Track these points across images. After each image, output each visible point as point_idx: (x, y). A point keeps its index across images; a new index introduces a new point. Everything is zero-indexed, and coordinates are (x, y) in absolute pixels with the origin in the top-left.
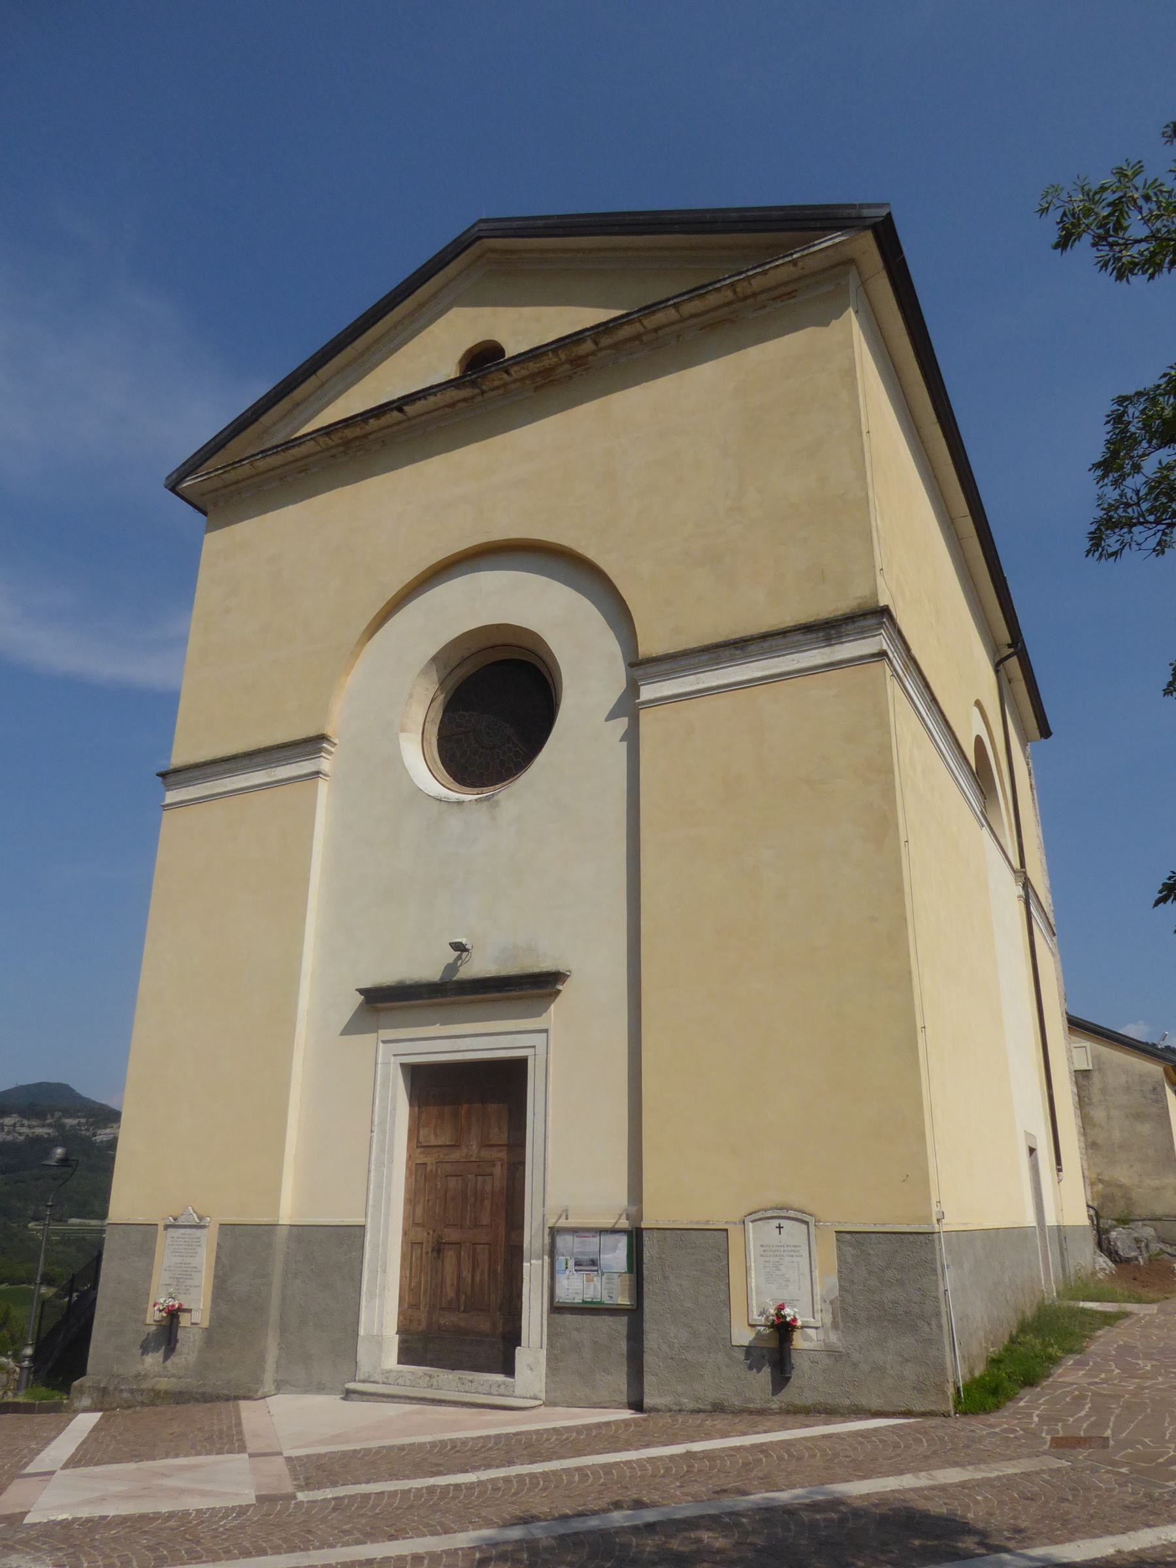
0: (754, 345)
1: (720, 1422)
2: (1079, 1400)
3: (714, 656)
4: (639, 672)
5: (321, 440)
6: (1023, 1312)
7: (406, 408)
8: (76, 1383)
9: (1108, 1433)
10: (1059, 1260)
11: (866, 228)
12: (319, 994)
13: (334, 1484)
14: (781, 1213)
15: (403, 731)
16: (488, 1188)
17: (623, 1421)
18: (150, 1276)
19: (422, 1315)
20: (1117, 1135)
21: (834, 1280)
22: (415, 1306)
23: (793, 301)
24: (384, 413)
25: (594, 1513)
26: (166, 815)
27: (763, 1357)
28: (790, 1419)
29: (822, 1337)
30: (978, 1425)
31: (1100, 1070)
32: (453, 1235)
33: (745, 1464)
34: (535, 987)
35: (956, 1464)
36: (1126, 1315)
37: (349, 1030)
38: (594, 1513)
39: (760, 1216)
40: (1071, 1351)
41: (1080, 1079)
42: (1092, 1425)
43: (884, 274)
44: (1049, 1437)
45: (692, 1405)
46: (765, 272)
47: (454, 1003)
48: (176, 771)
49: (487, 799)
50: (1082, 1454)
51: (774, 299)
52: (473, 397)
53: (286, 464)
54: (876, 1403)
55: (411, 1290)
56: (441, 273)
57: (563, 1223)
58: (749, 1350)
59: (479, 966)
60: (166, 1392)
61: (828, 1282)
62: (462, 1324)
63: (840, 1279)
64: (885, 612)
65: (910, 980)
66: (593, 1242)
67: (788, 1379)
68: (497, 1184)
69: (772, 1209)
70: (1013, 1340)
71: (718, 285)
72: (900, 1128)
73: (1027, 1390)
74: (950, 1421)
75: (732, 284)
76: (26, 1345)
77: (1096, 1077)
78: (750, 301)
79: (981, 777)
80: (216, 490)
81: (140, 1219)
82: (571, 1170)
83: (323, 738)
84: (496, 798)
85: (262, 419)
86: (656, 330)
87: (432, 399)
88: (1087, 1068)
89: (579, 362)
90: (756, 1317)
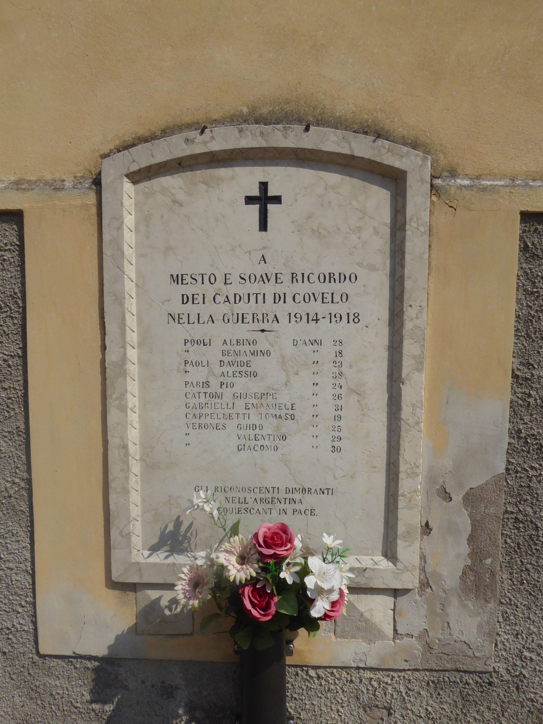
21: (491, 412)
27: (168, 692)
58: (107, 674)
61: (466, 424)
69: (236, 120)
90: (138, 553)
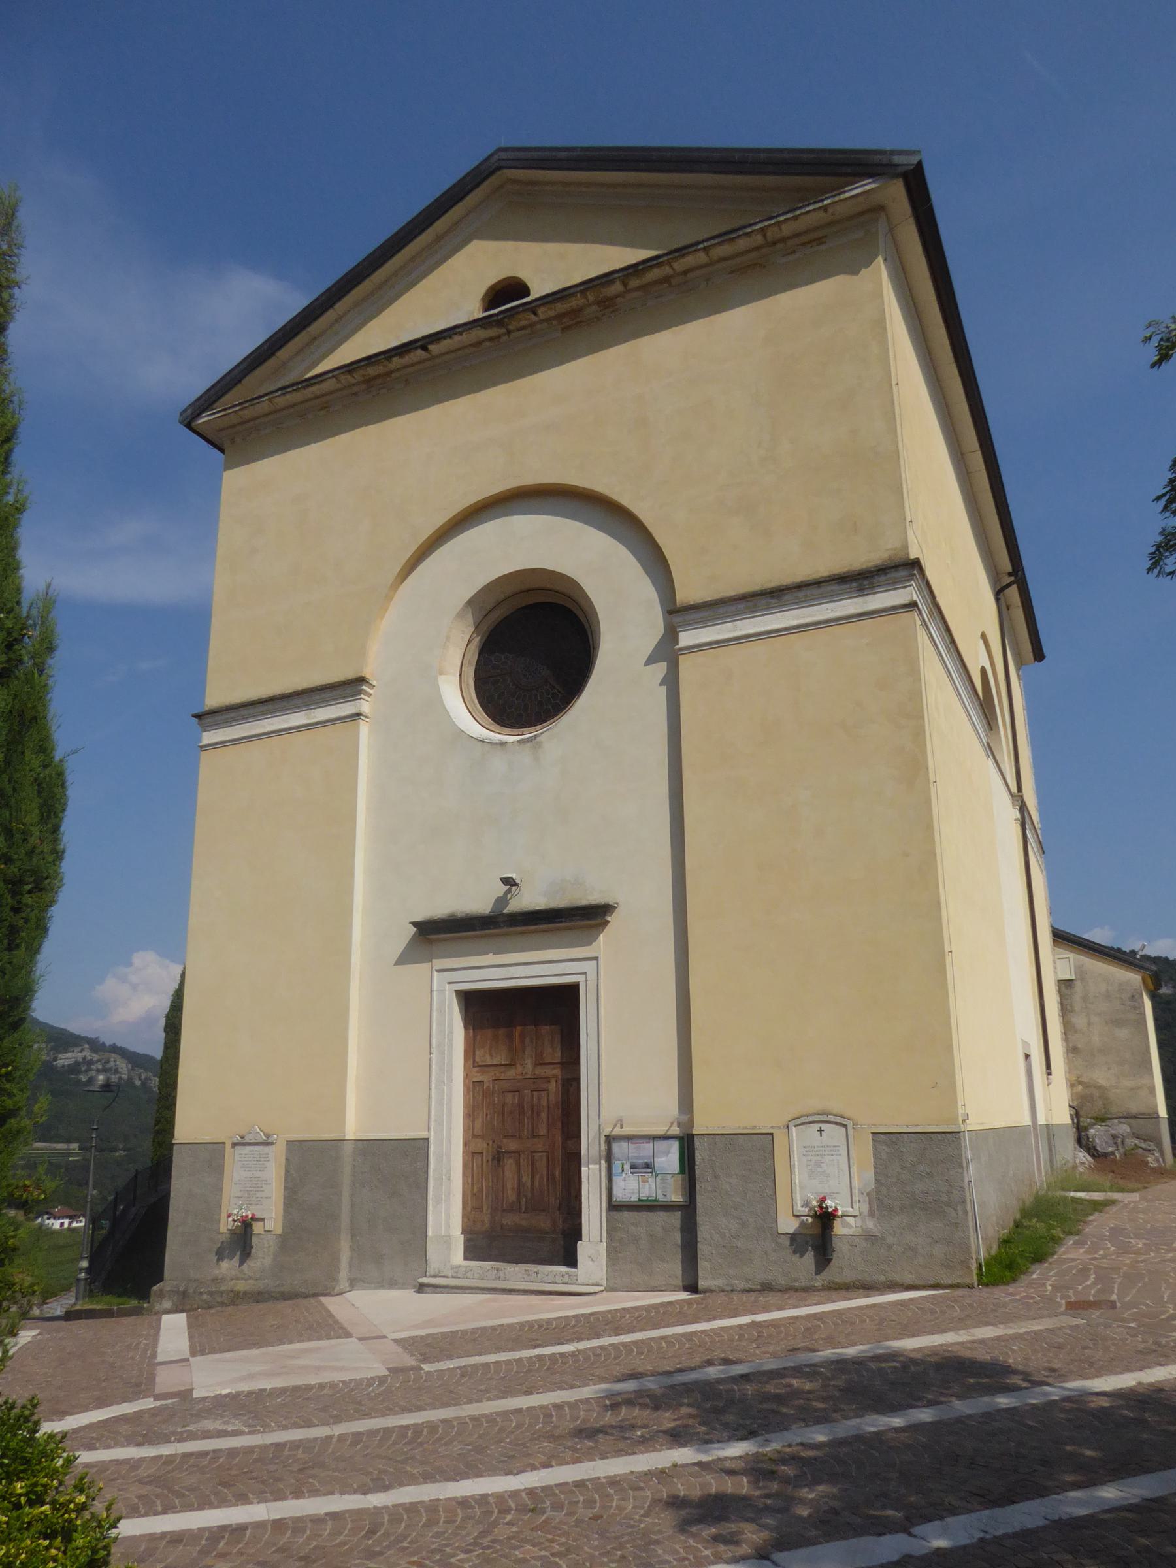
0: (785, 290)
1: (772, 1298)
2: (1084, 1272)
3: (750, 604)
4: (677, 619)
5: (342, 378)
6: (1024, 1202)
7: (430, 347)
8: (155, 1288)
9: (1114, 1297)
10: (1047, 1157)
11: (896, 176)
12: (372, 926)
13: (450, 1357)
14: (822, 1118)
15: (441, 673)
16: (544, 1102)
17: (684, 1300)
18: (221, 1190)
19: (486, 1219)
20: (1096, 1040)
21: (870, 1175)
22: (479, 1209)
23: (822, 247)
24: (409, 351)
25: (692, 1369)
26: (205, 757)
28: (834, 1294)
29: (859, 1223)
30: (999, 1294)
31: (1082, 980)
32: (512, 1145)
33: (807, 1329)
34: (588, 918)
35: (987, 1324)
36: (1113, 1202)
37: (402, 960)
38: (692, 1369)
39: (803, 1120)
40: (1070, 1233)
41: (1063, 989)
42: (1098, 1292)
43: (912, 221)
44: (1063, 1302)
45: (741, 1285)
46: (796, 218)
47: (506, 934)
48: (213, 712)
49: (530, 740)
50: (1095, 1314)
51: (803, 244)
52: (499, 337)
53: (307, 401)
54: (909, 1278)
55: (473, 1194)
56: (460, 204)
57: (617, 1131)
58: (793, 1237)
59: (529, 899)
60: (245, 1293)
61: (865, 1177)
62: (524, 1223)
63: (876, 1173)
64: (916, 564)
65: (940, 909)
66: (647, 1148)
67: (829, 1261)
68: (552, 1097)
69: (814, 1114)
70: (1017, 1225)
71: (749, 230)
72: (931, 1041)
73: (1037, 1266)
74: (975, 1292)
75: (762, 229)
76: (82, 1258)
77: (1078, 987)
78: (780, 246)
79: (985, 706)
80: (233, 426)
81: (207, 1138)
82: (624, 1084)
83: (362, 680)
84: (538, 739)
85: (278, 354)
86: (686, 272)
87: (457, 338)
88: (1068, 977)
89: (607, 304)
90: (800, 1209)
